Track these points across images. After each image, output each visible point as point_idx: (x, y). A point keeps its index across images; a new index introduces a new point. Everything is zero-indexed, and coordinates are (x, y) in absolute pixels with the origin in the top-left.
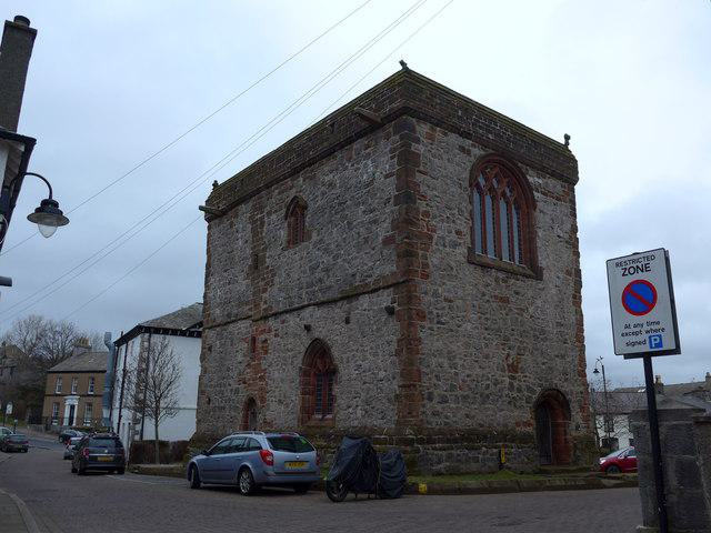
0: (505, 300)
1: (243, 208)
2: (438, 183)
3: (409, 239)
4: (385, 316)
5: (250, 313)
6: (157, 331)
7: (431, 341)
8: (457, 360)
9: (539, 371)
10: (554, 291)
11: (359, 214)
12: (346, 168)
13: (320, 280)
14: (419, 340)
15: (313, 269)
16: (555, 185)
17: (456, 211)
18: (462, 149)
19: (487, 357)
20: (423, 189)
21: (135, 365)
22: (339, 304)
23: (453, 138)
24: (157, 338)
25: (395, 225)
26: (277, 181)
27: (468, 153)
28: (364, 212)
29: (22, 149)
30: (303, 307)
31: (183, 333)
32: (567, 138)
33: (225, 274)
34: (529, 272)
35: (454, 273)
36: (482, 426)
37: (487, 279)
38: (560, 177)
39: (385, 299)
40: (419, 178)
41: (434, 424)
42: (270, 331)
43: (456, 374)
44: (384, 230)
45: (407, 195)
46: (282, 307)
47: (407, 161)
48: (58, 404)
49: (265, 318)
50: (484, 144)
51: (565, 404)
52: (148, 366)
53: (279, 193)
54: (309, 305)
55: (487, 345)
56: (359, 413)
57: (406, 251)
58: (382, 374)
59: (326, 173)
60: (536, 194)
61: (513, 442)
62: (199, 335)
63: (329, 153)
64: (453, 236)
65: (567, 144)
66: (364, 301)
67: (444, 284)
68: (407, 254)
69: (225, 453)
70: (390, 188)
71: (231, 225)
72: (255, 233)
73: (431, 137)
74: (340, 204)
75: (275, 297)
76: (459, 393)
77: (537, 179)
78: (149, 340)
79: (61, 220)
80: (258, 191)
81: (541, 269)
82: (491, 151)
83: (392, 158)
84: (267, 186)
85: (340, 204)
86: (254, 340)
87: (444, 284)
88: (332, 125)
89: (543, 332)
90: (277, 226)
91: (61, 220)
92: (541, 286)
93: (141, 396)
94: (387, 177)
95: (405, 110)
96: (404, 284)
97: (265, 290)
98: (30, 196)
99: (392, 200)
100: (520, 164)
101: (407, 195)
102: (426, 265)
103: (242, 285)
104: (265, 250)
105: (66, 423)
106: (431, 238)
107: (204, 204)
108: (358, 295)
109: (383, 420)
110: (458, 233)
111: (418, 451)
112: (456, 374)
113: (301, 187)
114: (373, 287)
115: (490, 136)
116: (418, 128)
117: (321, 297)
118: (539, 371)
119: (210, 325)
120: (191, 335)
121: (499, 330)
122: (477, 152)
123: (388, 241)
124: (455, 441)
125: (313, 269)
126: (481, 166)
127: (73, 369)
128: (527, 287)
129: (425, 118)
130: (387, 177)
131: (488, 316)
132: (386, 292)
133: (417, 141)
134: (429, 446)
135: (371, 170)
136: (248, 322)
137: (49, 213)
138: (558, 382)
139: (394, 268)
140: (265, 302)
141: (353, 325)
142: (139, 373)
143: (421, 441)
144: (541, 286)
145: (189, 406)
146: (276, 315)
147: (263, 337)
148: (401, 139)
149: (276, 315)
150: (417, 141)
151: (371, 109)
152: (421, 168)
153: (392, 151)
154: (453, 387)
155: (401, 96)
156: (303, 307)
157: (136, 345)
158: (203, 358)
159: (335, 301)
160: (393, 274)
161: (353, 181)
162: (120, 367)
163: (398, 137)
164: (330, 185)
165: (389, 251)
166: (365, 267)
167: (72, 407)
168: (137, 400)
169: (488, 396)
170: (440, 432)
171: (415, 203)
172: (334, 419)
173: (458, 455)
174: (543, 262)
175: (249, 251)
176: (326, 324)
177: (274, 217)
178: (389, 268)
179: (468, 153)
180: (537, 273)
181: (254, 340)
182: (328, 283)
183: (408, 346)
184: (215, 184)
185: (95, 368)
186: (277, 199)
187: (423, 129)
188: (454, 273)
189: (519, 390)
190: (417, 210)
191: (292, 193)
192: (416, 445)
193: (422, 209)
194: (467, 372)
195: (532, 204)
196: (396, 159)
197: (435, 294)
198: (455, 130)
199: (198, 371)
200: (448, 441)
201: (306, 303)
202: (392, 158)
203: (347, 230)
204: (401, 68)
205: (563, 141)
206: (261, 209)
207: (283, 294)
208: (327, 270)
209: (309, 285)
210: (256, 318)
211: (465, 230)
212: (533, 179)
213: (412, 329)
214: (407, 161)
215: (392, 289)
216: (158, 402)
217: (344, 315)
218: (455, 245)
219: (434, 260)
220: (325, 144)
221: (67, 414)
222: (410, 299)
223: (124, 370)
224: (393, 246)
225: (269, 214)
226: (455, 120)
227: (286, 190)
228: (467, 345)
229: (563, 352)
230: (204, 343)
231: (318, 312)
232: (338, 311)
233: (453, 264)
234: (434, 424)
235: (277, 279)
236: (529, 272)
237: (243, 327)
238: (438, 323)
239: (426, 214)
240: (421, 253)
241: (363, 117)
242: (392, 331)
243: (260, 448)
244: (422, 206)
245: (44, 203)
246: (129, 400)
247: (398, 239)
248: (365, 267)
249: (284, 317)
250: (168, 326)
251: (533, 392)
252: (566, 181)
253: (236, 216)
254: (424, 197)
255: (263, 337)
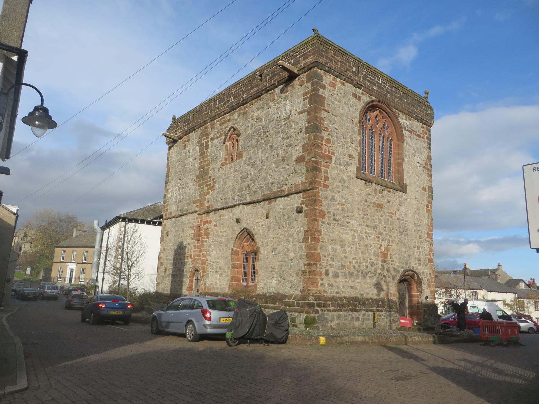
0: (380, 206)
1: (194, 134)
2: (337, 119)
3: (313, 161)
4: (295, 215)
5: (197, 209)
6: (130, 220)
7: (328, 232)
8: (346, 248)
9: (402, 257)
10: (414, 201)
11: (277, 140)
12: (270, 107)
13: (249, 187)
14: (320, 232)
15: (244, 178)
16: (417, 126)
17: (349, 140)
18: (355, 96)
19: (367, 246)
20: (326, 122)
21: (115, 244)
22: (262, 204)
23: (348, 86)
24: (131, 225)
25: (306, 148)
26: (219, 116)
27: (359, 98)
28: (283, 138)
29: (15, 58)
30: (235, 206)
31: (148, 223)
32: (426, 93)
33: (180, 182)
34: (399, 188)
35: (346, 185)
36: (362, 295)
37: (369, 190)
38: (421, 120)
39: (297, 200)
40: (324, 114)
41: (329, 293)
42: (210, 222)
43: (345, 257)
44: (297, 152)
45: (314, 127)
46: (219, 206)
47: (316, 101)
48: (63, 268)
49: (208, 212)
50: (370, 92)
51: (420, 282)
52: (123, 244)
53: (220, 125)
54: (239, 205)
55: (367, 237)
56: (275, 282)
57: (313, 167)
58: (292, 255)
59: (255, 110)
60: (404, 132)
61: (382, 307)
62: (160, 224)
63: (258, 96)
64: (347, 158)
65: (426, 98)
66: (281, 202)
67: (339, 192)
68: (313, 169)
69: (177, 310)
70: (302, 121)
71: (185, 147)
72: (202, 153)
73: (333, 85)
74: (265, 133)
75: (215, 198)
76: (347, 271)
77: (404, 121)
78: (125, 227)
79: (52, 125)
80: (205, 123)
81: (406, 185)
82: (374, 98)
83: (305, 99)
84: (212, 119)
85: (265, 133)
86: (199, 228)
87: (339, 192)
88: (261, 76)
89: (406, 229)
90: (217, 148)
91: (52, 125)
92: (405, 197)
93: (118, 265)
94: (300, 113)
95: (316, 64)
96: (309, 190)
97: (208, 193)
98: (27, 102)
99: (304, 130)
100: (394, 110)
101: (314, 127)
102: (327, 178)
103: (192, 189)
104: (209, 164)
105: (67, 281)
106: (331, 158)
107: (165, 132)
108: (276, 198)
109: (292, 287)
110: (350, 156)
111: (317, 312)
112: (345, 257)
113: (236, 119)
114: (286, 192)
115: (375, 88)
116: (324, 78)
117: (248, 199)
118: (402, 257)
119: (167, 217)
120: (154, 224)
121: (375, 227)
122: (366, 98)
123: (300, 160)
124: (344, 305)
125: (244, 178)
126: (370, 108)
127: (73, 245)
128: (395, 197)
129: (329, 71)
130: (300, 113)
131: (368, 216)
132: (297, 196)
133: (324, 87)
134: (325, 309)
135: (288, 108)
136: (196, 215)
137: (42, 118)
138: (414, 265)
139: (304, 180)
140: (208, 202)
141: (271, 219)
142: (117, 250)
143: (319, 305)
144: (405, 197)
145: (371, 317)
146: (215, 210)
147: (205, 227)
148: (312, 85)
149: (215, 210)
150: (324, 87)
151: (290, 63)
152: (326, 108)
153: (305, 94)
154: (343, 267)
155: (313, 54)
156: (235, 206)
157: (115, 230)
158: (162, 240)
159: (259, 202)
160: (303, 183)
161: (275, 116)
162: (104, 244)
163: (309, 84)
164: (258, 119)
165: (302, 168)
166: (282, 178)
167: (72, 271)
168: (116, 268)
169: (367, 274)
170: (333, 299)
171: (320, 132)
172: (255, 286)
173: (345, 316)
174: (407, 181)
175: (197, 165)
176: (253, 218)
177: (216, 141)
178: (300, 179)
179: (359, 98)
180: (403, 188)
181: (199, 228)
182: (254, 189)
183: (312, 235)
184: (174, 118)
185: (88, 245)
186: (217, 128)
187: (328, 79)
188: (346, 185)
189: (388, 270)
190: (322, 138)
191: (230, 125)
192: (316, 308)
193: (325, 137)
194: (354, 256)
195: (401, 138)
196: (307, 100)
197: (333, 199)
198: (350, 81)
199: (158, 248)
200: (339, 305)
201: (238, 203)
202: (305, 99)
203: (270, 152)
204: (312, 34)
205: (423, 95)
206: (207, 135)
207: (220, 196)
208: (253, 180)
209: (240, 190)
210: (202, 212)
211: (356, 155)
212: (403, 120)
213: (316, 223)
214: (316, 101)
215: (301, 194)
216: (129, 269)
217: (265, 212)
218: (349, 164)
219: (333, 173)
220: (255, 89)
221: (68, 276)
222: (314, 201)
223: (107, 247)
224: (304, 163)
225: (212, 139)
226: (351, 74)
227: (225, 123)
228: (354, 237)
229: (418, 245)
230: (163, 229)
231: (247, 209)
232: (263, 207)
233: (345, 178)
234: (329, 293)
235: (216, 186)
236: (399, 188)
237: (191, 220)
238: (334, 219)
239: (328, 141)
240: (323, 169)
241: (284, 68)
242: (300, 224)
243: (201, 307)
244: (325, 135)
245: (36, 109)
246: (109, 267)
247: (307, 158)
248: (282, 178)
249: (221, 212)
250: (138, 217)
251: (398, 272)
252: (424, 124)
253: (188, 141)
254: (326, 129)
255: (205, 227)
